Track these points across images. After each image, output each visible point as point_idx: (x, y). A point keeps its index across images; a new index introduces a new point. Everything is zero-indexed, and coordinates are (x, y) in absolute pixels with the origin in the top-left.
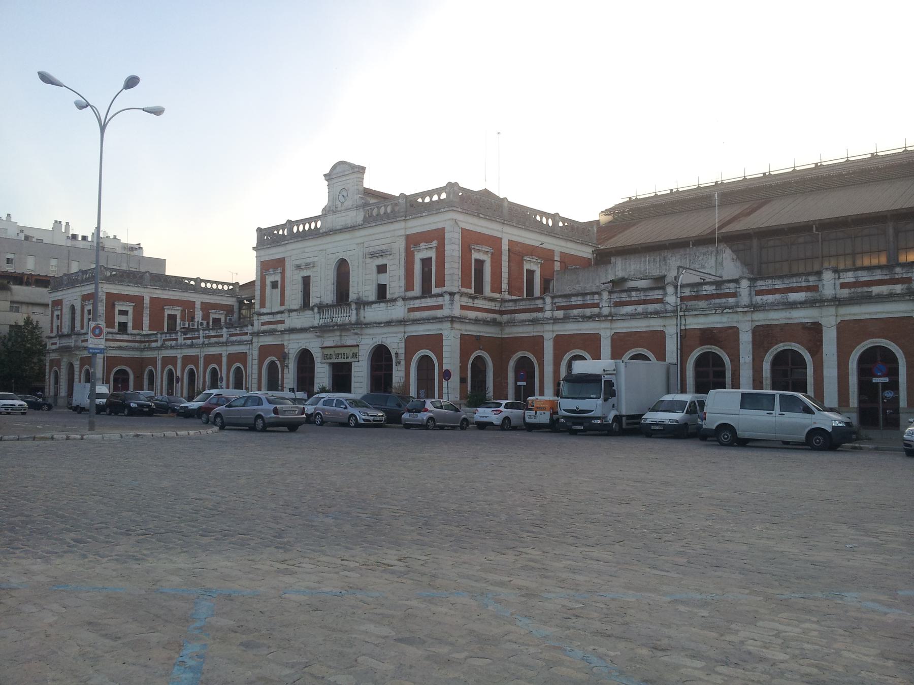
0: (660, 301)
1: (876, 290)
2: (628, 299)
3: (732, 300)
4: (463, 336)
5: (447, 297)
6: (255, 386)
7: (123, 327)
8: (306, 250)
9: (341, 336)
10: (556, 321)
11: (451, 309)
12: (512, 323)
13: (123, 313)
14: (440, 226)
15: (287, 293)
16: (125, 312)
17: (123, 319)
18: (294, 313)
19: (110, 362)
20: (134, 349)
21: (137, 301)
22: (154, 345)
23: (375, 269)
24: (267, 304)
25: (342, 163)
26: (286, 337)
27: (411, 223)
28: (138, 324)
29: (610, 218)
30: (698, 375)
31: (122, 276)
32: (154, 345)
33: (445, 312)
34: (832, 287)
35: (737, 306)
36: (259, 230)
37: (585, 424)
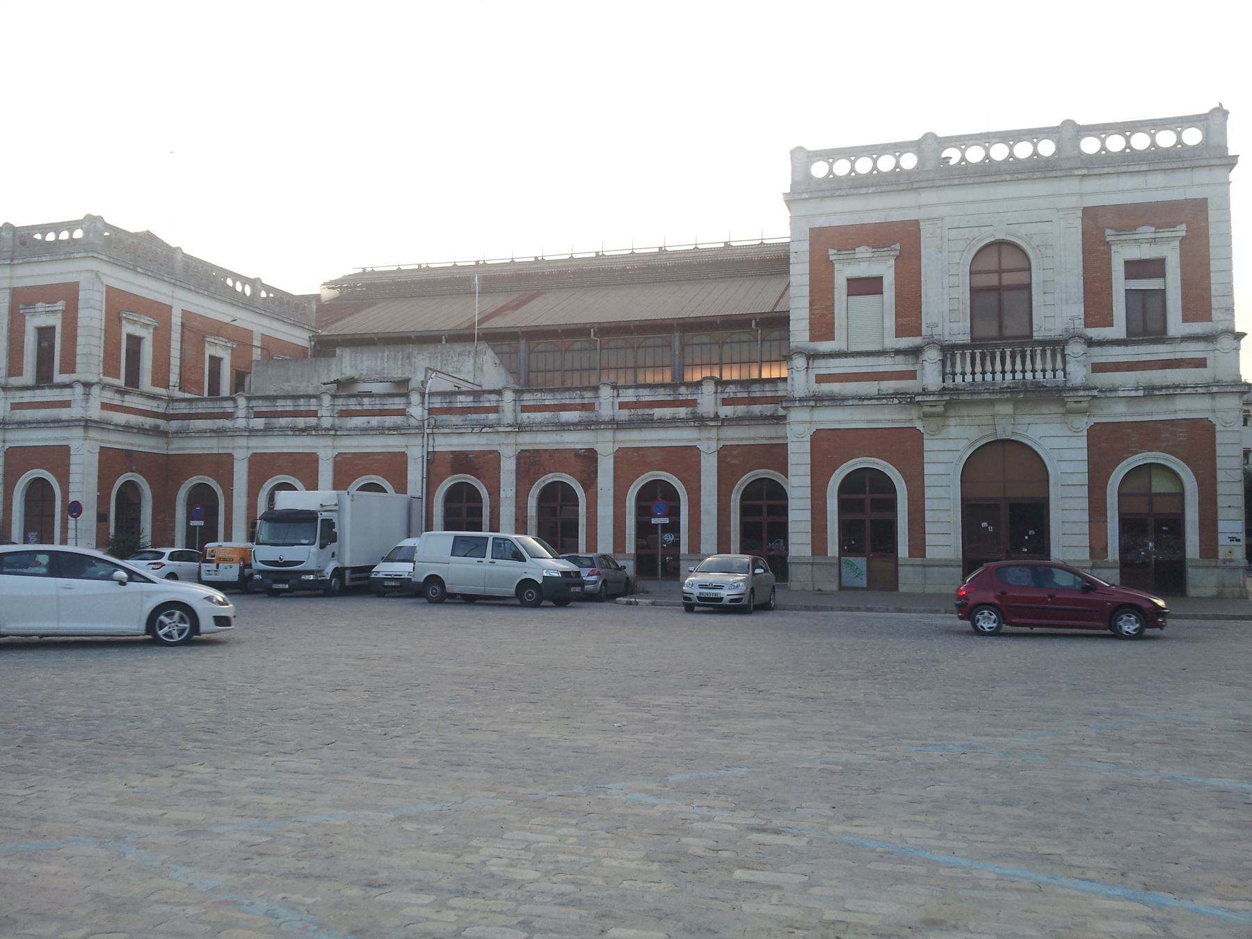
0: (402, 413)
1: (658, 412)
2: (358, 408)
3: (492, 416)
4: (104, 451)
5: (79, 390)
10: (252, 432)
11: (86, 408)
12: (182, 433)
33: (75, 412)
35: (499, 424)
37: (292, 582)
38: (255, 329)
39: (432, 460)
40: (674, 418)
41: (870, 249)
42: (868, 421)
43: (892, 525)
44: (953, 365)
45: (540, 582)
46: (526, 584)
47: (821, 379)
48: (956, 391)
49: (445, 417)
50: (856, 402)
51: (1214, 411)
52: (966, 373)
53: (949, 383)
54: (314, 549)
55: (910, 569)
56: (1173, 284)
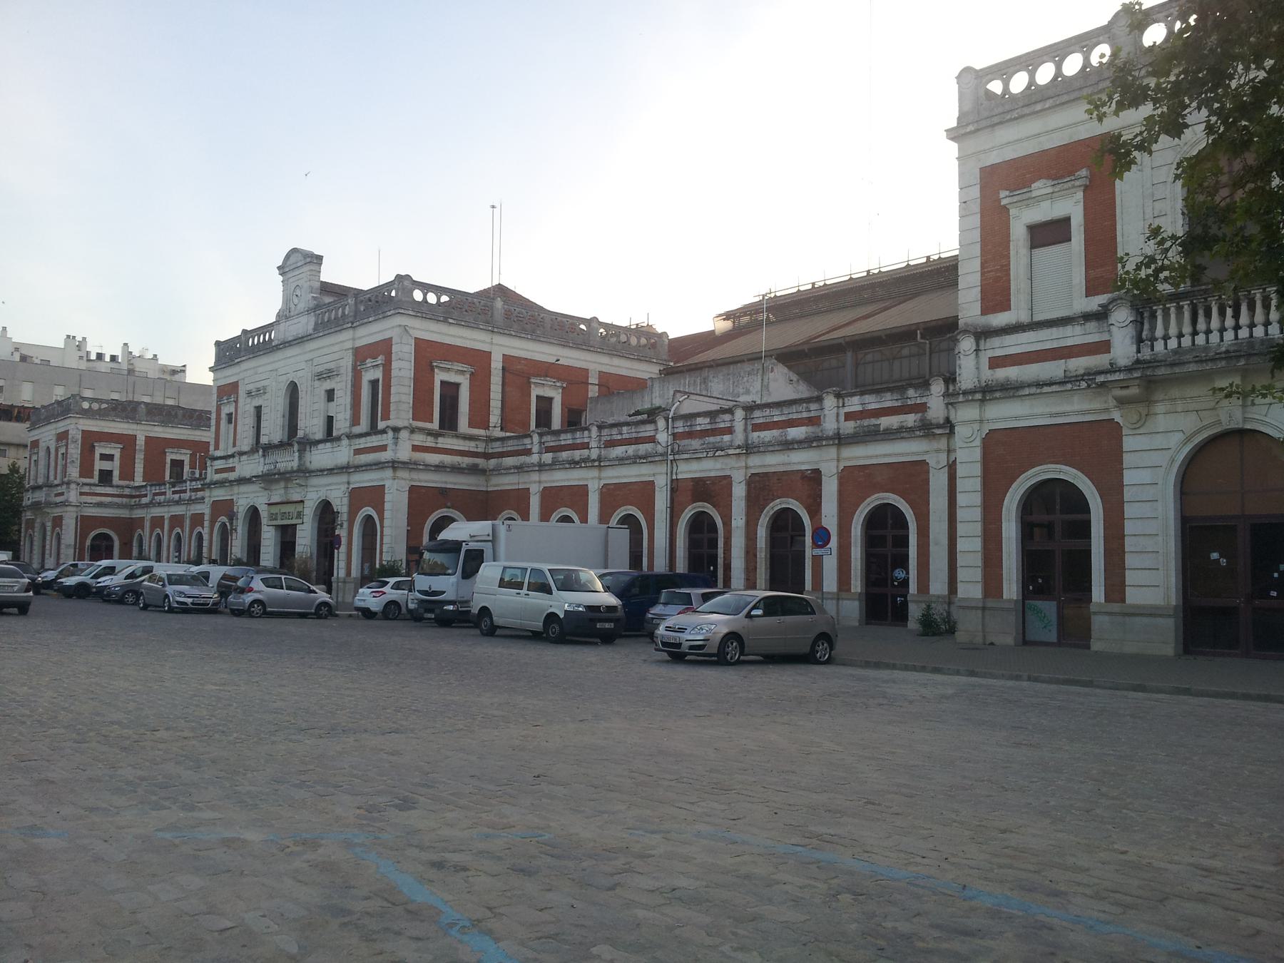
0: (652, 440)
1: (885, 422)
2: (619, 437)
3: (727, 438)
4: (413, 490)
5: (391, 434)
6: (153, 554)
7: (106, 477)
8: (260, 370)
9: (286, 488)
10: (541, 467)
11: (395, 451)
12: (498, 471)
13: (105, 457)
14: (387, 335)
15: (239, 428)
16: (109, 457)
17: (106, 465)
18: (244, 458)
19: (85, 523)
20: (119, 506)
21: (128, 442)
22: (144, 500)
23: (323, 396)
24: (222, 445)
25: (294, 251)
26: (236, 489)
27: (361, 332)
28: (127, 473)
29: (728, 325)
30: (93, 547)
31: (114, 409)
32: (144, 500)
33: (386, 456)
34: (834, 419)
35: (730, 447)
36: (218, 344)
37: (437, 611)
38: (591, 367)
39: (675, 487)
40: (902, 427)
41: (1050, 182)
42: (1051, 415)
43: (1085, 557)
44: (1153, 329)
45: (562, 616)
46: (551, 617)
47: (995, 363)
48: (1154, 363)
49: (686, 442)
50: (1033, 390)
52: (1173, 333)
53: (1146, 354)
54: (453, 579)
55: (1106, 618)
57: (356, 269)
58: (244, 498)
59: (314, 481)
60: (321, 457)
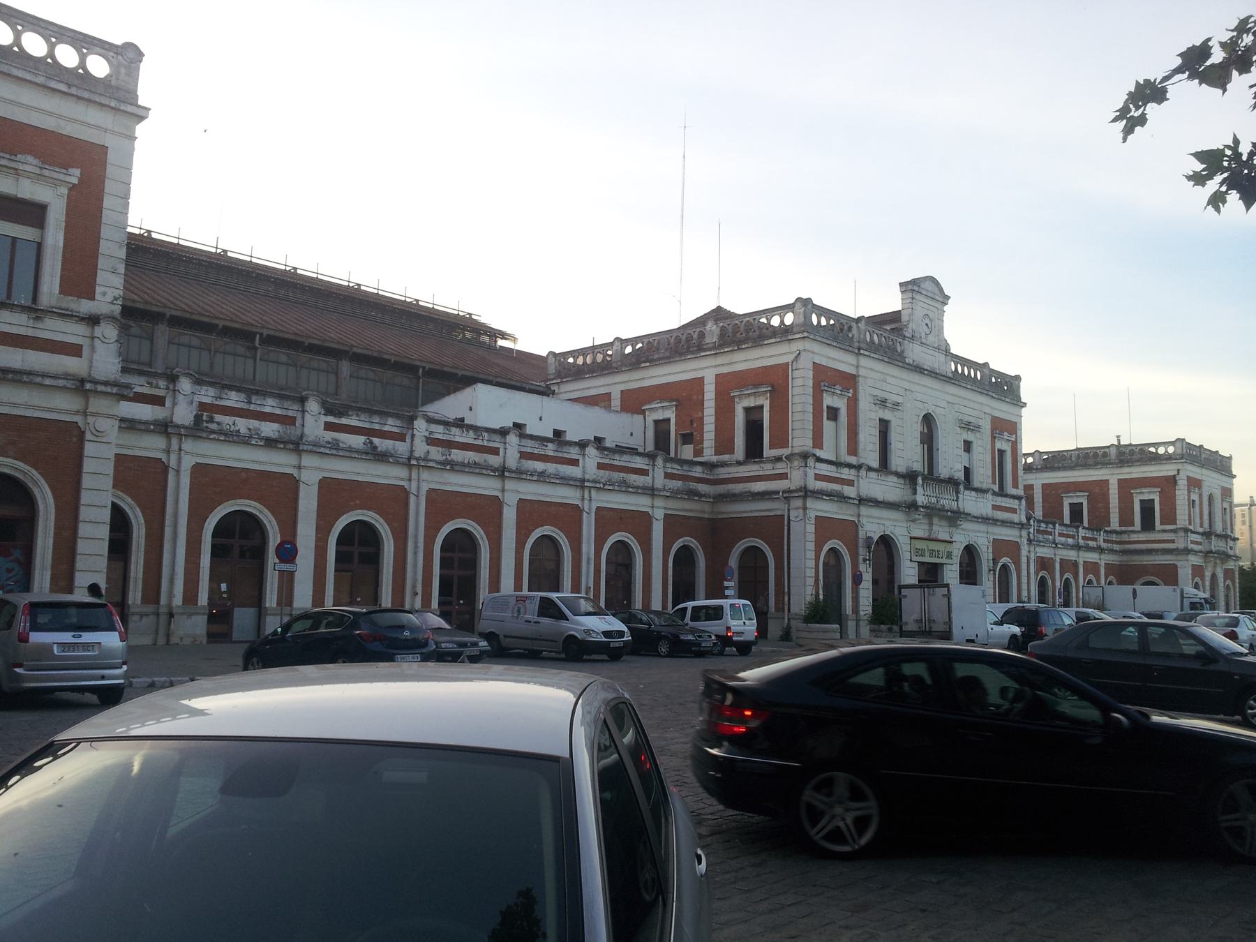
8: (890, 380)
51: (85, 414)
56: (55, 237)
57: (968, 334)
58: (874, 524)
59: (966, 525)
60: (969, 502)
